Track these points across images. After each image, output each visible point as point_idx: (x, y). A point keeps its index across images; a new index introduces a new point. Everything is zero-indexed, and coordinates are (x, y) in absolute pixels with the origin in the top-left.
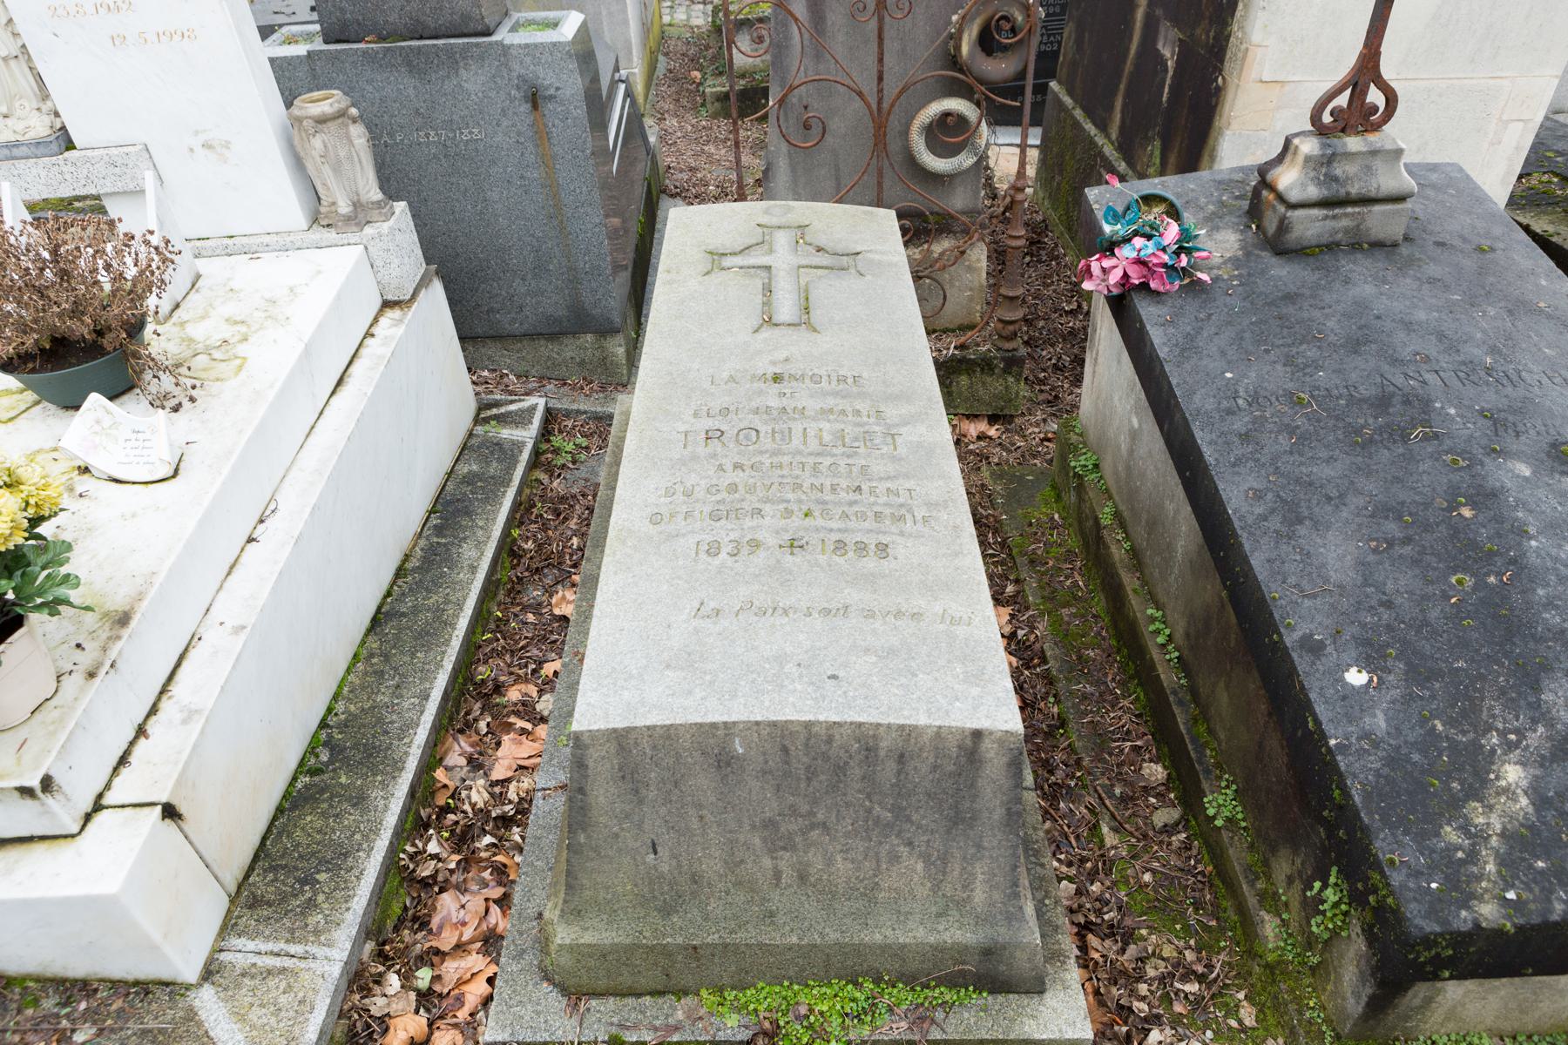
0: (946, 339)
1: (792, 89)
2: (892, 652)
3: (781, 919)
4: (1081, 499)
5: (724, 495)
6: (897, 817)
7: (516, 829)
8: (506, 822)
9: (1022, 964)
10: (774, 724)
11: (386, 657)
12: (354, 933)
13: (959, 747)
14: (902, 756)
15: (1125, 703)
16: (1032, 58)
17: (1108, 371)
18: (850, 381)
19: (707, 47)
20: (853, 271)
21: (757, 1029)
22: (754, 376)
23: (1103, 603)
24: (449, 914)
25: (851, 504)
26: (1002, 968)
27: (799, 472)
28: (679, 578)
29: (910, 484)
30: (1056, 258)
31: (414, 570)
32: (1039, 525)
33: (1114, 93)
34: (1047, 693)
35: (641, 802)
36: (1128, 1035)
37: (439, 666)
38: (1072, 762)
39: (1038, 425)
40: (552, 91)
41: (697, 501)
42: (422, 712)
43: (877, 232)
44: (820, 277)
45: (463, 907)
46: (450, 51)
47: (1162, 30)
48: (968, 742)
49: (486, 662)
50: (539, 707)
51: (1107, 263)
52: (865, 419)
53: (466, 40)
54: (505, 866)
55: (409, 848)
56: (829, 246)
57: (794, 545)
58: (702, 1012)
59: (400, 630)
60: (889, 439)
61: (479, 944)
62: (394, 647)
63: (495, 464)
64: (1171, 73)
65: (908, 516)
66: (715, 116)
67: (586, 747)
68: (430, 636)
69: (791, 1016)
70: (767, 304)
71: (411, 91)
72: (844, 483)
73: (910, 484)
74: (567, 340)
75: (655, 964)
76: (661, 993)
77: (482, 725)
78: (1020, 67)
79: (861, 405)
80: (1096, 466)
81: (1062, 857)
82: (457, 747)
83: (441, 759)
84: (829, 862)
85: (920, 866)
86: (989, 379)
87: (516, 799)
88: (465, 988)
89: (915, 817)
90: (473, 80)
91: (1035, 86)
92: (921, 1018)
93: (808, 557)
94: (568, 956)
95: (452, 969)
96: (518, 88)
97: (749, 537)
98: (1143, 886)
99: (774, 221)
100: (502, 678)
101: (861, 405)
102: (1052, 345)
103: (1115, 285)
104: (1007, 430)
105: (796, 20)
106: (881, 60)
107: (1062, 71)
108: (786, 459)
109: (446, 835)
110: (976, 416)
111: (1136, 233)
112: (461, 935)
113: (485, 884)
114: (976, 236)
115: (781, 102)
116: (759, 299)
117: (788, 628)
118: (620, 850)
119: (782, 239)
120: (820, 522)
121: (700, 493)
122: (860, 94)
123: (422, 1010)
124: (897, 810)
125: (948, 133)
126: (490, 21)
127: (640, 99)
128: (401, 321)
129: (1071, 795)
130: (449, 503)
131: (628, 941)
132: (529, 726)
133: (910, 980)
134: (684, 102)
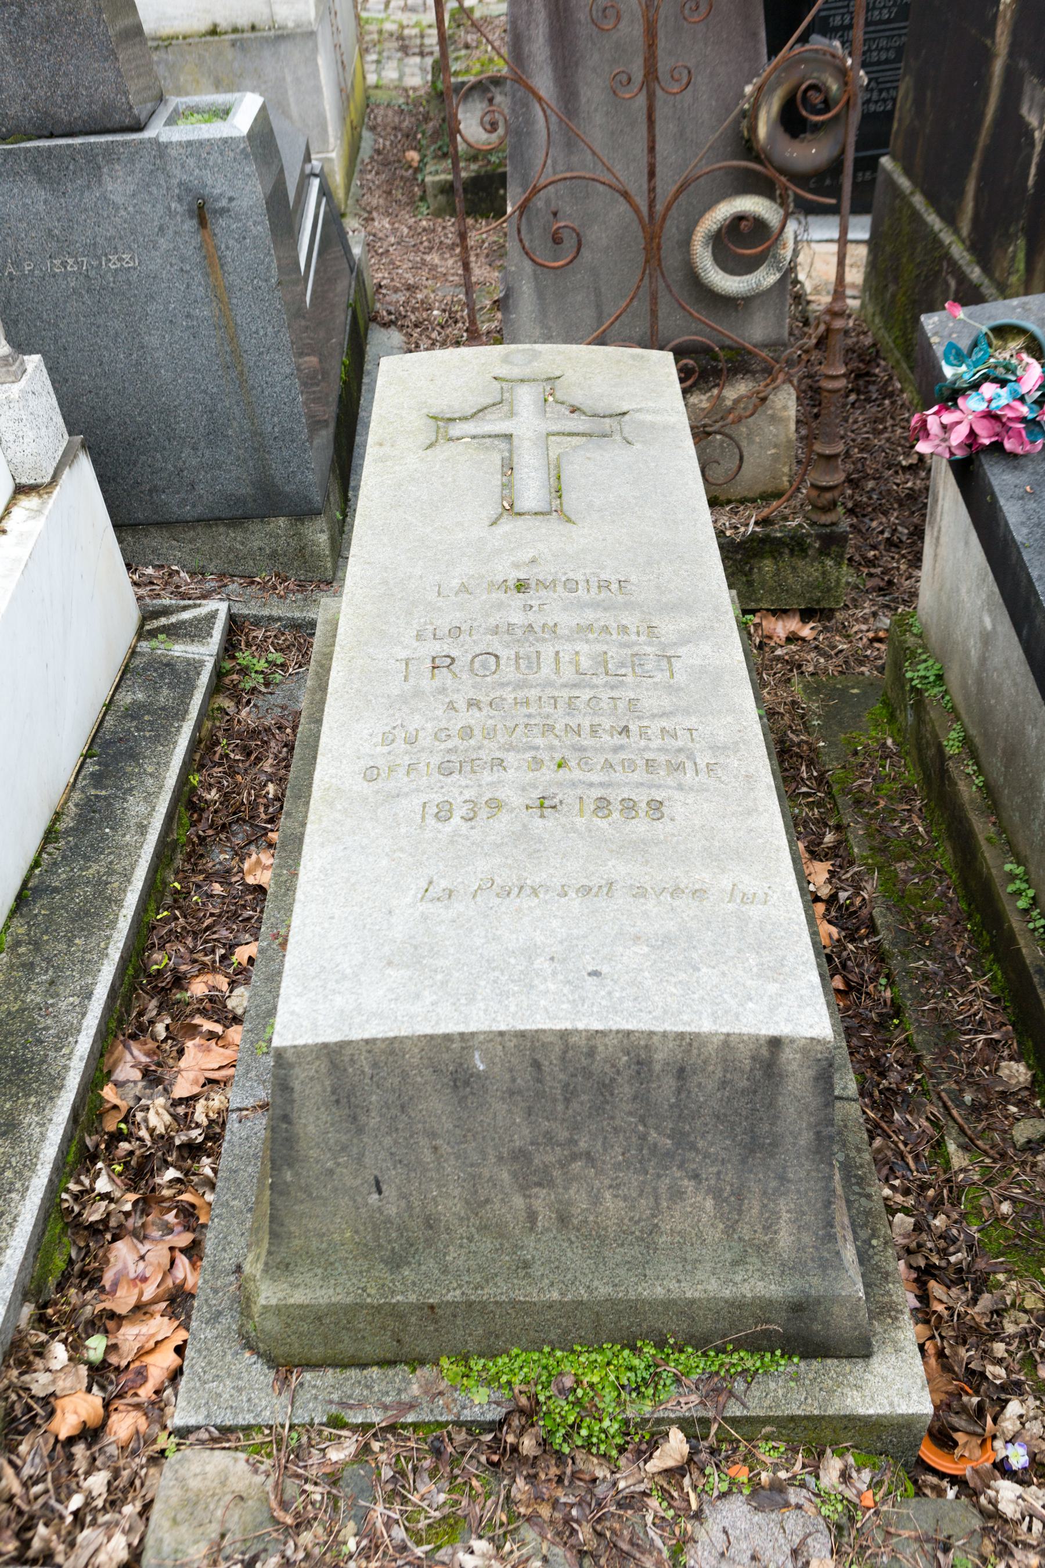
0: (744, 512)
1: (536, 191)
2: (667, 940)
3: (537, 1270)
4: (920, 720)
5: (455, 742)
6: (678, 1145)
7: (206, 1161)
8: (193, 1150)
9: (841, 1322)
10: (522, 1034)
11: (37, 946)
12: (8, 1294)
13: (753, 1058)
14: (682, 1070)
15: (978, 984)
16: (852, 139)
17: (951, 560)
18: (614, 587)
19: (427, 119)
20: (617, 437)
21: (511, 1406)
22: (491, 584)
23: (950, 855)
24: (125, 1267)
25: (616, 749)
26: (817, 1327)
27: (550, 710)
28: (402, 850)
29: (692, 722)
30: (890, 395)
31: (68, 832)
32: (867, 754)
33: (964, 176)
34: (878, 973)
35: (360, 1131)
36: (980, 1406)
37: (103, 954)
38: (909, 1061)
39: (865, 620)
40: (224, 203)
41: (423, 750)
42: (84, 1015)
43: (648, 383)
44: (575, 448)
45: (142, 1258)
46: (88, 152)
47: (1027, 89)
48: (765, 1052)
49: (162, 948)
50: (230, 1004)
51: (948, 418)
52: (634, 637)
53: (110, 138)
54: (193, 1206)
55: (73, 1187)
56: (586, 404)
57: (544, 805)
58: (443, 1386)
59: (53, 910)
60: (664, 663)
61: (164, 1305)
62: (46, 932)
63: (165, 691)
64: (1038, 148)
65: (689, 765)
66: (438, 213)
67: (291, 1066)
68: (92, 915)
69: (553, 1390)
70: (508, 486)
71: (41, 207)
72: (607, 723)
73: (692, 722)
74: (255, 526)
75: (384, 1328)
76: (392, 1363)
77: (160, 1029)
78: (836, 153)
79: (630, 620)
80: (940, 677)
81: (897, 1183)
82: (128, 1057)
83: (110, 1073)
84: (596, 1200)
85: (709, 1203)
86: (801, 564)
87: (205, 1122)
88: (148, 1360)
89: (701, 1144)
90: (118, 186)
91: (856, 161)
92: (716, 1390)
93: (563, 820)
94: (275, 1319)
95: (130, 1336)
96: (180, 199)
97: (488, 795)
98: (1000, 1219)
99: (516, 372)
100: (183, 968)
101: (630, 620)
102: (885, 513)
103: (959, 446)
104: (826, 629)
105: (540, 99)
106: (652, 149)
107: (897, 141)
108: (533, 693)
109: (119, 1168)
110: (785, 612)
111: (986, 378)
112: (141, 1294)
113: (169, 1230)
114: (781, 377)
115: (523, 208)
116: (497, 480)
117: (538, 912)
118: (335, 1190)
119: (526, 397)
120: (577, 774)
121: (425, 740)
122: (625, 195)
123: (95, 1388)
124: (680, 1137)
125: (743, 242)
126: (140, 111)
127: (340, 193)
128: (39, 511)
129: (909, 1104)
130: (108, 744)
131: (349, 1300)
132: (218, 1028)
133: (702, 1343)
134: (398, 194)
